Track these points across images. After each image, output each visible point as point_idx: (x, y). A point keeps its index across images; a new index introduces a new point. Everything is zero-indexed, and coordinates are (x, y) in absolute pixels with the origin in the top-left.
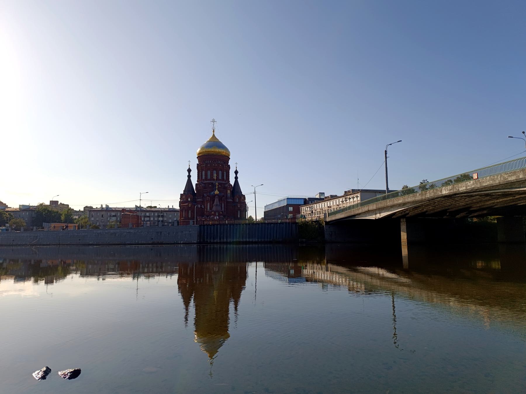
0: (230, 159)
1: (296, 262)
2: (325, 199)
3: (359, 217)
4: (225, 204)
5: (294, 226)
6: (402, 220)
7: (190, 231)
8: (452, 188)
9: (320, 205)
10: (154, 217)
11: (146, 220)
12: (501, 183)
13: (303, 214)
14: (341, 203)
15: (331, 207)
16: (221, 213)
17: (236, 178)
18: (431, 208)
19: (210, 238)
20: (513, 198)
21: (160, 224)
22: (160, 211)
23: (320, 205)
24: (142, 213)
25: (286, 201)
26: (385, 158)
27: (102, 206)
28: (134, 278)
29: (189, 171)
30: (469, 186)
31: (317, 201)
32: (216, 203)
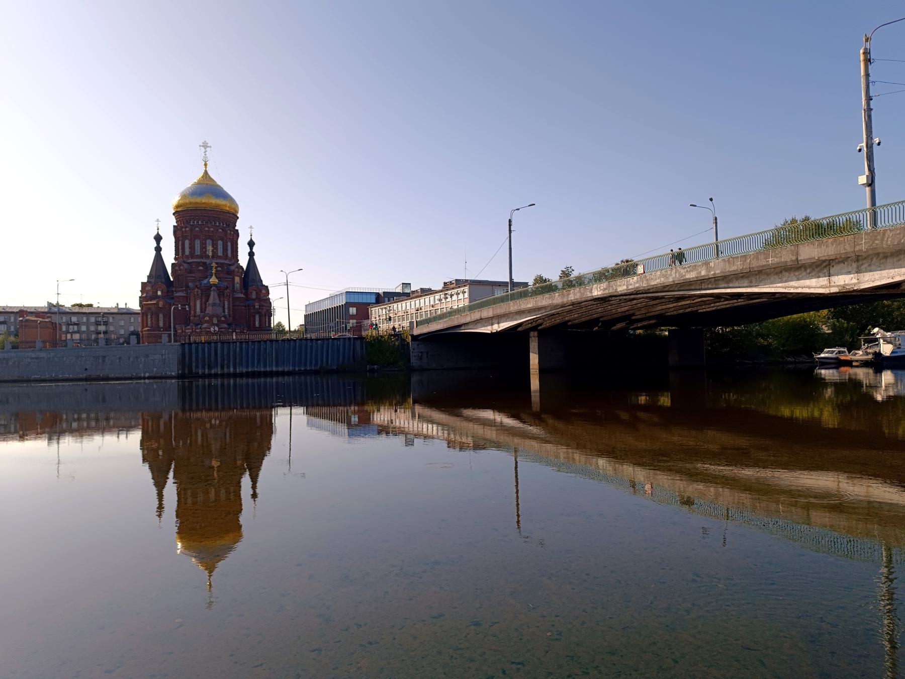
0: (238, 218)
1: (362, 404)
2: (411, 295)
3: (466, 328)
4: (231, 302)
5: (358, 343)
6: (532, 334)
7: (162, 355)
8: (607, 286)
9: (404, 305)
10: (88, 324)
11: (71, 331)
12: (676, 282)
13: (374, 319)
14: (437, 302)
15: (421, 309)
16: (223, 319)
17: (251, 254)
18: (576, 316)
19: (203, 367)
20: (692, 302)
21: (102, 343)
22: (100, 313)
23: (404, 305)
24: (62, 318)
25: (344, 297)
26: (508, 232)
28: (50, 439)
29: (158, 238)
30: (631, 284)
31: (398, 298)
32: (214, 300)
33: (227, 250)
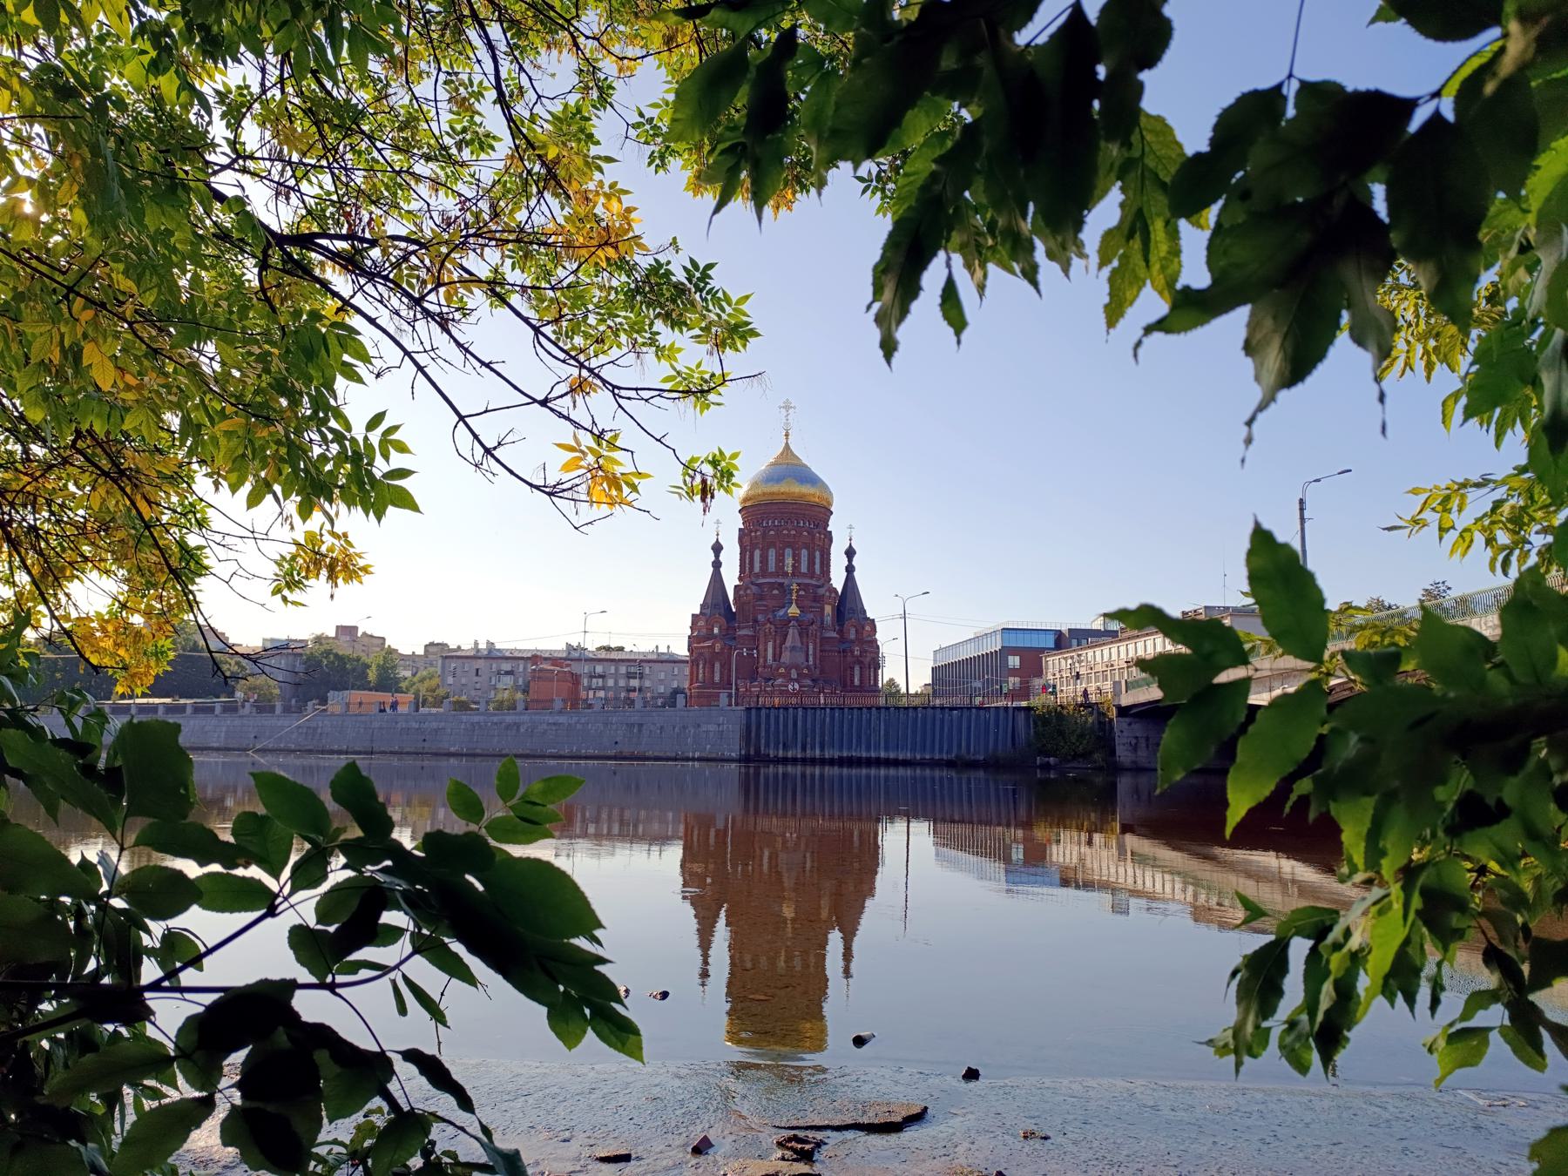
9: (1106, 652)
10: (616, 676)
16: (805, 671)
17: (850, 569)
23: (1106, 652)
25: (999, 637)
26: (1298, 521)
27: (476, 643)
29: (717, 548)
33: (814, 564)
